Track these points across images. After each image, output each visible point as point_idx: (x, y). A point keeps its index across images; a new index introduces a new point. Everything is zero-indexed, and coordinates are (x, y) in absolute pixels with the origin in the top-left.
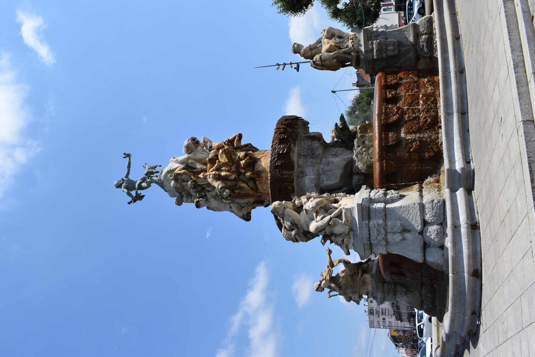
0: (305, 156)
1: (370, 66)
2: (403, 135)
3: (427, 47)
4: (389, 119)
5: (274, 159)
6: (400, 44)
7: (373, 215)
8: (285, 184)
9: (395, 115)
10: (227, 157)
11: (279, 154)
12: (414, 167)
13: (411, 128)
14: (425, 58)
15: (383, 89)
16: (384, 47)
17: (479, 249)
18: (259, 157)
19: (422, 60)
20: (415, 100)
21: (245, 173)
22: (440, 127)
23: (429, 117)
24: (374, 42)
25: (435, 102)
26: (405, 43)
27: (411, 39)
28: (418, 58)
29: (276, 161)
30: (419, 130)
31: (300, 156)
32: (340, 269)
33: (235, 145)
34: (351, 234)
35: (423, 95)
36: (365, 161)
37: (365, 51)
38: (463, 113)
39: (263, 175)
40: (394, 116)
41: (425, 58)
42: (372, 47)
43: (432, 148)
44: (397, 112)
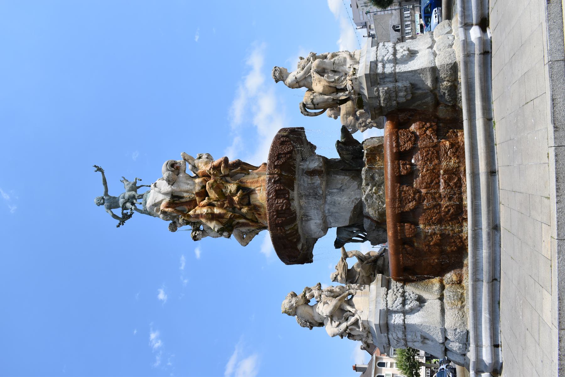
0: (307, 196)
2: (421, 226)
3: (449, 95)
4: (405, 206)
5: (273, 216)
6: (413, 86)
7: (391, 328)
8: (290, 239)
9: (412, 201)
10: (216, 192)
11: (277, 211)
12: (434, 260)
13: (431, 219)
15: (396, 160)
16: (394, 94)
17: (498, 289)
18: (253, 188)
19: (441, 107)
20: (432, 183)
21: (240, 209)
22: (466, 220)
23: (452, 206)
24: (381, 89)
25: (460, 185)
26: (421, 86)
27: (429, 83)
28: (437, 104)
29: (276, 218)
30: (440, 221)
31: (300, 196)
32: (352, 262)
33: (223, 172)
34: (370, 335)
35: (445, 172)
36: (376, 208)
38: (495, 280)
39: (262, 210)
40: (410, 202)
41: (446, 106)
42: (379, 94)
43: (454, 242)
44: (414, 199)
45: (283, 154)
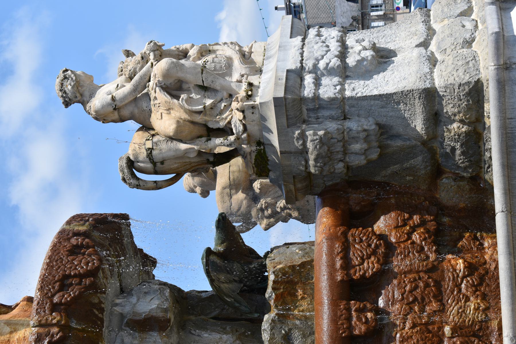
1: (299, 186)
14: (458, 178)
15: (341, 298)
16: (339, 147)
27: (419, 124)
28: (437, 172)
35: (454, 330)
37: (281, 152)
41: (458, 178)
42: (304, 144)
45: (75, 276)
